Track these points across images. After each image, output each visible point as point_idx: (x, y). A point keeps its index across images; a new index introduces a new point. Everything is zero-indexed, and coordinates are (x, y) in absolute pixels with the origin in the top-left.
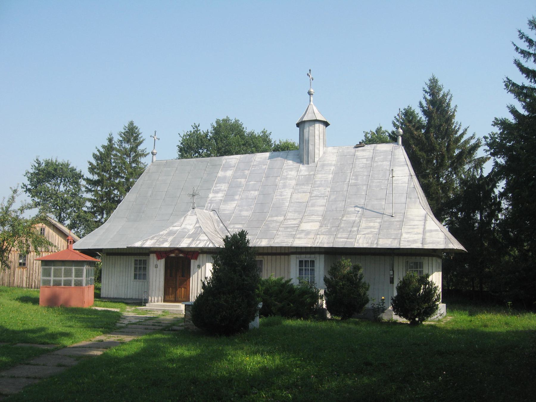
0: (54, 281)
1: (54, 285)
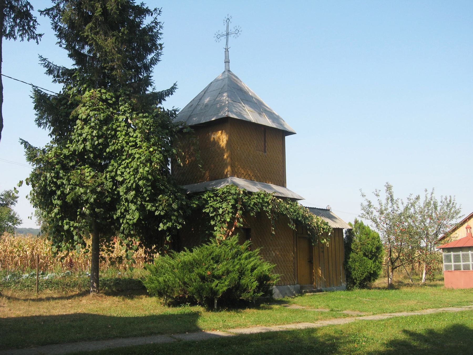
0: (455, 266)
1: (455, 270)
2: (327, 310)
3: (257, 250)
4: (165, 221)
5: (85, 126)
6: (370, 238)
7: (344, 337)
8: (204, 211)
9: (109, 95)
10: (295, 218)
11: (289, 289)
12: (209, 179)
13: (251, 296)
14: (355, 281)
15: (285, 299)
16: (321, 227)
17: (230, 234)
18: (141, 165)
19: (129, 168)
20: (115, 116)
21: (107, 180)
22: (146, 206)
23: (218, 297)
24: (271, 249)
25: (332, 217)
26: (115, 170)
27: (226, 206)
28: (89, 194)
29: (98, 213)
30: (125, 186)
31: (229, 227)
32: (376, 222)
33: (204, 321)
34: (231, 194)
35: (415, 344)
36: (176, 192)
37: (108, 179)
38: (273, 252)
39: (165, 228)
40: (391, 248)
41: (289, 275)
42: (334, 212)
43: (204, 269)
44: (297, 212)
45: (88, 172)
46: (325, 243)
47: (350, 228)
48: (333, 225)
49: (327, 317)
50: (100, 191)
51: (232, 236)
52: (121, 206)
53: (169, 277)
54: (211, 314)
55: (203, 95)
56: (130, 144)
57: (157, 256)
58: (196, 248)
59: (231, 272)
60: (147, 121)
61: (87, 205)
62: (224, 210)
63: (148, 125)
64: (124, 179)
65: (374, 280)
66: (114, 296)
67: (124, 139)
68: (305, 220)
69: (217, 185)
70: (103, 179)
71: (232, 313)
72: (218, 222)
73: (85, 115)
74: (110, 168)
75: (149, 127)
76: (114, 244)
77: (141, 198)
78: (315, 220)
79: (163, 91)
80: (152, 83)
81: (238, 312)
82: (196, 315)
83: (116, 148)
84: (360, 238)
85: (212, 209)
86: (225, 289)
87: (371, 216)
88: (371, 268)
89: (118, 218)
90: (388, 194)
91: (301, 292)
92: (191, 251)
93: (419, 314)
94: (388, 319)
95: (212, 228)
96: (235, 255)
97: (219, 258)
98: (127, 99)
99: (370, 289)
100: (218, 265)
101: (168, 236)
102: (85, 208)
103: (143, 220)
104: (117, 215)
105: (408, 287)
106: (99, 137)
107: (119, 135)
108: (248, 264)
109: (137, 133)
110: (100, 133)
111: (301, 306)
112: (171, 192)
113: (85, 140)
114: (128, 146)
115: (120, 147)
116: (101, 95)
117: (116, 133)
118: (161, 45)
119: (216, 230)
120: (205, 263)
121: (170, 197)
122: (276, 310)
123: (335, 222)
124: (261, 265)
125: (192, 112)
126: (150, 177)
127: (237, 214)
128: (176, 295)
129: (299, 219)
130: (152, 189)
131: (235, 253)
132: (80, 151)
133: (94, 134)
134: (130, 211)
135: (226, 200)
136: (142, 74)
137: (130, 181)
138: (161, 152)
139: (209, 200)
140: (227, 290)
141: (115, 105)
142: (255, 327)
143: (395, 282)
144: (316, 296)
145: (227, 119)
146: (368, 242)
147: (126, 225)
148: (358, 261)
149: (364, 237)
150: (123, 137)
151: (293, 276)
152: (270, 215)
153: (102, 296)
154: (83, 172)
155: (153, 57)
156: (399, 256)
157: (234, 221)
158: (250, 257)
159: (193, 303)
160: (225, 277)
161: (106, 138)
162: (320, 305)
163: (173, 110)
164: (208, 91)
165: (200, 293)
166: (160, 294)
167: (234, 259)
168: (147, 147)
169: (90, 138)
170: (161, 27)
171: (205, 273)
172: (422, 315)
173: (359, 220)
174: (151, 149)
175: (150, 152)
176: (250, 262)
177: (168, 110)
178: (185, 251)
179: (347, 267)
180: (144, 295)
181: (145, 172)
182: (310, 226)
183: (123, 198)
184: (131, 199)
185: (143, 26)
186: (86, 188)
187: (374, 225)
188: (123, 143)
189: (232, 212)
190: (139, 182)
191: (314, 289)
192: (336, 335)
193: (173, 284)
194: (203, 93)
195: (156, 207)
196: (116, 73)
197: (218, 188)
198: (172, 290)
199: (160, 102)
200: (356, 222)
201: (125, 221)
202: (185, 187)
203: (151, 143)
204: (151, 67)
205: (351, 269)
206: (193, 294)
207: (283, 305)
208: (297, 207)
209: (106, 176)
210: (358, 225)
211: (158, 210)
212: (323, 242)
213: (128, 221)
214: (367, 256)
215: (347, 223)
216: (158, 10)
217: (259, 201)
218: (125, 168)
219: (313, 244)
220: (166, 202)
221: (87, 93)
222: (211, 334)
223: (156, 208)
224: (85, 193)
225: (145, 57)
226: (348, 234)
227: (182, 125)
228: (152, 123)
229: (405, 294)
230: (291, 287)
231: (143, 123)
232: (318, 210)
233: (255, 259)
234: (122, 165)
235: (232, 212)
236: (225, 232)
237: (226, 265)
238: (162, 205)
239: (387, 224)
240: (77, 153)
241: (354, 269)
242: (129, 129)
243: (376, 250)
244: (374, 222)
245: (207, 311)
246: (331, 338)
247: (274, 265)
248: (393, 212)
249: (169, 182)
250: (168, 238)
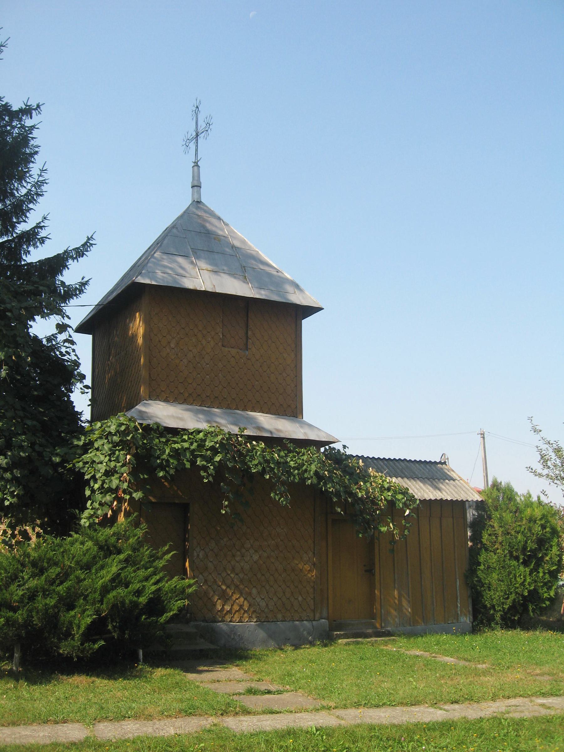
205: (483, 586)
214: (517, 558)
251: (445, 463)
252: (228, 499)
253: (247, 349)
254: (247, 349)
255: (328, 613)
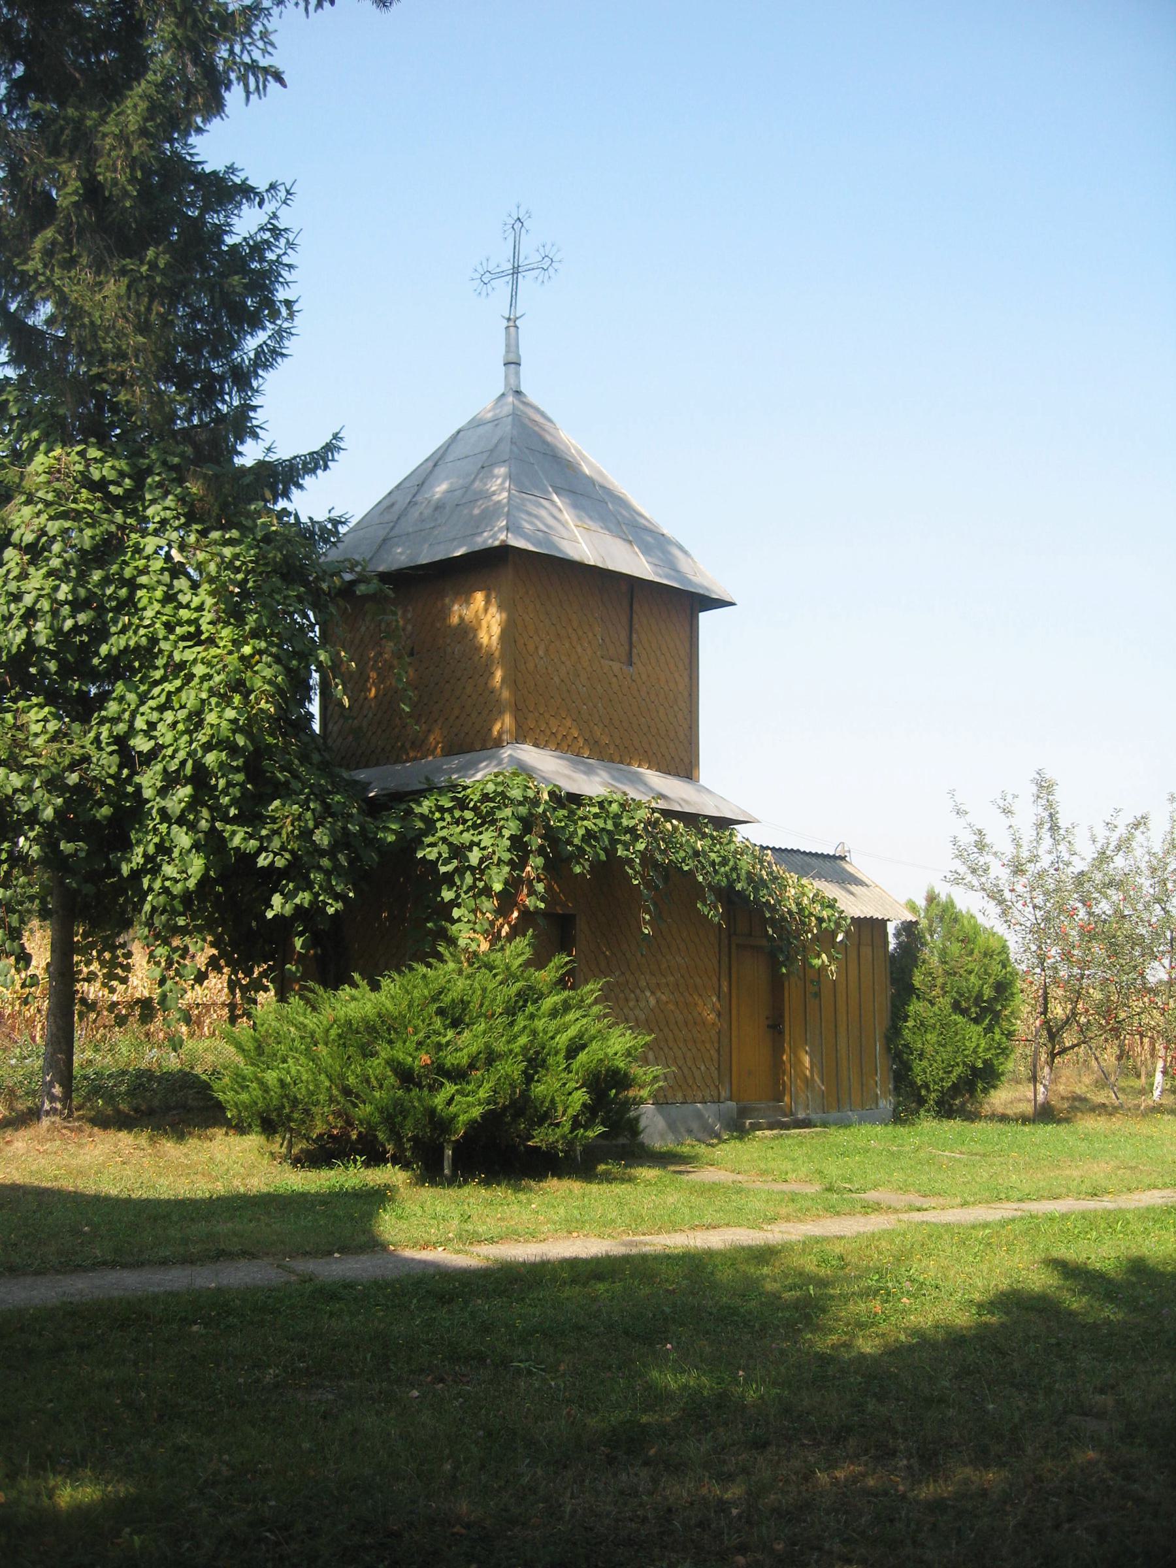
2: (814, 1188)
3: (592, 989)
4: (291, 885)
5: (32, 570)
6: (976, 951)
7: (847, 1279)
8: (420, 855)
9: (113, 468)
10: (724, 883)
11: (699, 1116)
12: (442, 748)
13: (564, 1137)
14: (923, 1092)
15: (685, 1150)
16: (811, 914)
17: (503, 933)
18: (214, 700)
19: (172, 709)
20: (133, 536)
21: (100, 749)
22: (226, 835)
23: (453, 1139)
24: (643, 984)
25: (847, 880)
26: (126, 716)
27: (492, 841)
28: (39, 793)
29: (71, 856)
30: (159, 767)
31: (502, 911)
32: (1001, 902)
33: (400, 1218)
34: (512, 800)
35: (1075, 1306)
36: (329, 792)
37: (103, 745)
38: (648, 994)
39: (288, 910)
40: (1046, 987)
41: (703, 1068)
42: (857, 865)
43: (411, 1046)
44: (731, 863)
45: (38, 721)
46: (823, 967)
47: (911, 917)
48: (854, 906)
49: (808, 1210)
50: (77, 785)
51: (510, 938)
52: (147, 833)
53: (298, 1067)
54: (427, 1193)
55: (431, 472)
56: (179, 630)
57: (266, 998)
58: (390, 977)
59: (500, 1056)
60: (236, 556)
61: (32, 829)
62: (485, 853)
63: (238, 570)
64: (157, 744)
65: (985, 1091)
66: (120, 1130)
67: (158, 612)
68: (756, 890)
69: (464, 769)
70: (89, 746)
71: (500, 1192)
72: (466, 893)
73: (32, 531)
74: (113, 708)
75: (240, 576)
76: (129, 955)
77: (210, 808)
78: (793, 891)
79: (295, 458)
80: (258, 430)
81: (517, 1189)
82: (380, 1197)
83: (132, 643)
84: (944, 953)
85: (444, 850)
86: (476, 1112)
87: (983, 880)
88: (975, 1052)
89: (136, 875)
90: (1040, 809)
91: (739, 1128)
92: (375, 987)
93: (1110, 1206)
94: (1004, 1223)
95: (444, 911)
96: (516, 1002)
97: (464, 1010)
98: (173, 480)
99: (973, 1121)
100: (459, 1033)
101: (301, 934)
102: (27, 838)
103: (216, 881)
104: (134, 865)
105: (1099, 1115)
106: (77, 605)
107: (144, 601)
108: (557, 1032)
109: (204, 596)
110: (82, 592)
111: (733, 1171)
112: (312, 793)
113: (31, 614)
114: (172, 637)
115: (144, 641)
116: (87, 466)
117: (132, 594)
118: (288, 304)
119: (459, 920)
120: (415, 1027)
121: (308, 809)
122: (648, 1183)
123: (852, 894)
124: (601, 1036)
125: (392, 528)
126: (241, 740)
127: (528, 869)
128: (318, 1131)
129: (739, 887)
130: (249, 779)
131: (516, 995)
132: (14, 650)
133: (61, 596)
134: (176, 854)
135: (493, 822)
136: (227, 397)
137: (176, 751)
138: (278, 659)
139: (438, 820)
140: (483, 1116)
141: (131, 502)
142: (567, 1238)
143: (1063, 1098)
144: (788, 1142)
145: (504, 553)
146: (970, 967)
147: (162, 899)
148: (934, 1028)
149: (955, 948)
150: (157, 606)
151: (715, 1074)
152: (636, 873)
153: (80, 1130)
154: (23, 719)
155: (265, 342)
156: (1074, 1014)
157: (518, 891)
158: (566, 1007)
159: (375, 1158)
160: (479, 1073)
161: (101, 610)
162: (794, 1171)
163: (330, 520)
164: (450, 457)
165: (393, 1124)
166: (269, 1126)
167: (514, 1014)
168: (234, 642)
169: (47, 607)
170: (290, 245)
171: (414, 1058)
172: (1121, 1210)
173: (944, 891)
174: (247, 650)
175: (242, 658)
176: (566, 1027)
177: (311, 519)
178: (356, 986)
179: (896, 1047)
180: (221, 1125)
181: (224, 724)
182: (773, 909)
183: (153, 807)
184: (178, 813)
185: (230, 240)
186: (30, 774)
187: (993, 909)
188: (157, 626)
189: (511, 862)
190: (203, 756)
191: (786, 1116)
192: (824, 1272)
193: (312, 1094)
194: (431, 464)
195: (261, 839)
196: (128, 397)
197: (468, 782)
198: (307, 1111)
199: (286, 494)
200: (932, 898)
201: (157, 885)
202: (362, 775)
203: (247, 628)
204: (257, 376)
205: (912, 1054)
206: (372, 1128)
207: (672, 1168)
208: (732, 847)
209: (99, 734)
210: (936, 911)
211: (266, 850)
212: (817, 962)
213: (167, 883)
214: (964, 1012)
215: (903, 901)
216: (282, 188)
217: (602, 825)
218: (161, 709)
219: (784, 971)
220: (292, 825)
221: (40, 458)
222: (413, 1260)
223: (262, 844)
224: (27, 790)
225: (235, 346)
226: (903, 938)
227: (352, 571)
228: (251, 561)
229: (1086, 1138)
230: (709, 1112)
231: (223, 562)
232: (806, 858)
233: (584, 1016)
234: (152, 698)
235: (511, 862)
236: (487, 926)
237: (485, 1032)
238: (280, 834)
239: (1035, 907)
240: (4, 658)
241: (921, 1055)
242: (176, 582)
243: (993, 994)
244: (994, 898)
245: (417, 1184)
246: (806, 1279)
247: (648, 1038)
248: (1056, 870)
249: (304, 758)
250: (298, 943)
251: (843, 858)
252: (648, 912)
253: (631, 664)
254: (631, 664)
255: (731, 1091)
